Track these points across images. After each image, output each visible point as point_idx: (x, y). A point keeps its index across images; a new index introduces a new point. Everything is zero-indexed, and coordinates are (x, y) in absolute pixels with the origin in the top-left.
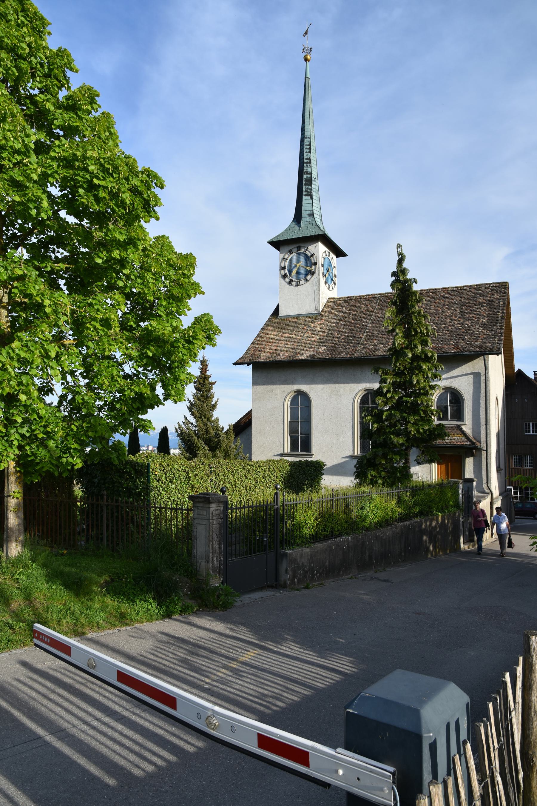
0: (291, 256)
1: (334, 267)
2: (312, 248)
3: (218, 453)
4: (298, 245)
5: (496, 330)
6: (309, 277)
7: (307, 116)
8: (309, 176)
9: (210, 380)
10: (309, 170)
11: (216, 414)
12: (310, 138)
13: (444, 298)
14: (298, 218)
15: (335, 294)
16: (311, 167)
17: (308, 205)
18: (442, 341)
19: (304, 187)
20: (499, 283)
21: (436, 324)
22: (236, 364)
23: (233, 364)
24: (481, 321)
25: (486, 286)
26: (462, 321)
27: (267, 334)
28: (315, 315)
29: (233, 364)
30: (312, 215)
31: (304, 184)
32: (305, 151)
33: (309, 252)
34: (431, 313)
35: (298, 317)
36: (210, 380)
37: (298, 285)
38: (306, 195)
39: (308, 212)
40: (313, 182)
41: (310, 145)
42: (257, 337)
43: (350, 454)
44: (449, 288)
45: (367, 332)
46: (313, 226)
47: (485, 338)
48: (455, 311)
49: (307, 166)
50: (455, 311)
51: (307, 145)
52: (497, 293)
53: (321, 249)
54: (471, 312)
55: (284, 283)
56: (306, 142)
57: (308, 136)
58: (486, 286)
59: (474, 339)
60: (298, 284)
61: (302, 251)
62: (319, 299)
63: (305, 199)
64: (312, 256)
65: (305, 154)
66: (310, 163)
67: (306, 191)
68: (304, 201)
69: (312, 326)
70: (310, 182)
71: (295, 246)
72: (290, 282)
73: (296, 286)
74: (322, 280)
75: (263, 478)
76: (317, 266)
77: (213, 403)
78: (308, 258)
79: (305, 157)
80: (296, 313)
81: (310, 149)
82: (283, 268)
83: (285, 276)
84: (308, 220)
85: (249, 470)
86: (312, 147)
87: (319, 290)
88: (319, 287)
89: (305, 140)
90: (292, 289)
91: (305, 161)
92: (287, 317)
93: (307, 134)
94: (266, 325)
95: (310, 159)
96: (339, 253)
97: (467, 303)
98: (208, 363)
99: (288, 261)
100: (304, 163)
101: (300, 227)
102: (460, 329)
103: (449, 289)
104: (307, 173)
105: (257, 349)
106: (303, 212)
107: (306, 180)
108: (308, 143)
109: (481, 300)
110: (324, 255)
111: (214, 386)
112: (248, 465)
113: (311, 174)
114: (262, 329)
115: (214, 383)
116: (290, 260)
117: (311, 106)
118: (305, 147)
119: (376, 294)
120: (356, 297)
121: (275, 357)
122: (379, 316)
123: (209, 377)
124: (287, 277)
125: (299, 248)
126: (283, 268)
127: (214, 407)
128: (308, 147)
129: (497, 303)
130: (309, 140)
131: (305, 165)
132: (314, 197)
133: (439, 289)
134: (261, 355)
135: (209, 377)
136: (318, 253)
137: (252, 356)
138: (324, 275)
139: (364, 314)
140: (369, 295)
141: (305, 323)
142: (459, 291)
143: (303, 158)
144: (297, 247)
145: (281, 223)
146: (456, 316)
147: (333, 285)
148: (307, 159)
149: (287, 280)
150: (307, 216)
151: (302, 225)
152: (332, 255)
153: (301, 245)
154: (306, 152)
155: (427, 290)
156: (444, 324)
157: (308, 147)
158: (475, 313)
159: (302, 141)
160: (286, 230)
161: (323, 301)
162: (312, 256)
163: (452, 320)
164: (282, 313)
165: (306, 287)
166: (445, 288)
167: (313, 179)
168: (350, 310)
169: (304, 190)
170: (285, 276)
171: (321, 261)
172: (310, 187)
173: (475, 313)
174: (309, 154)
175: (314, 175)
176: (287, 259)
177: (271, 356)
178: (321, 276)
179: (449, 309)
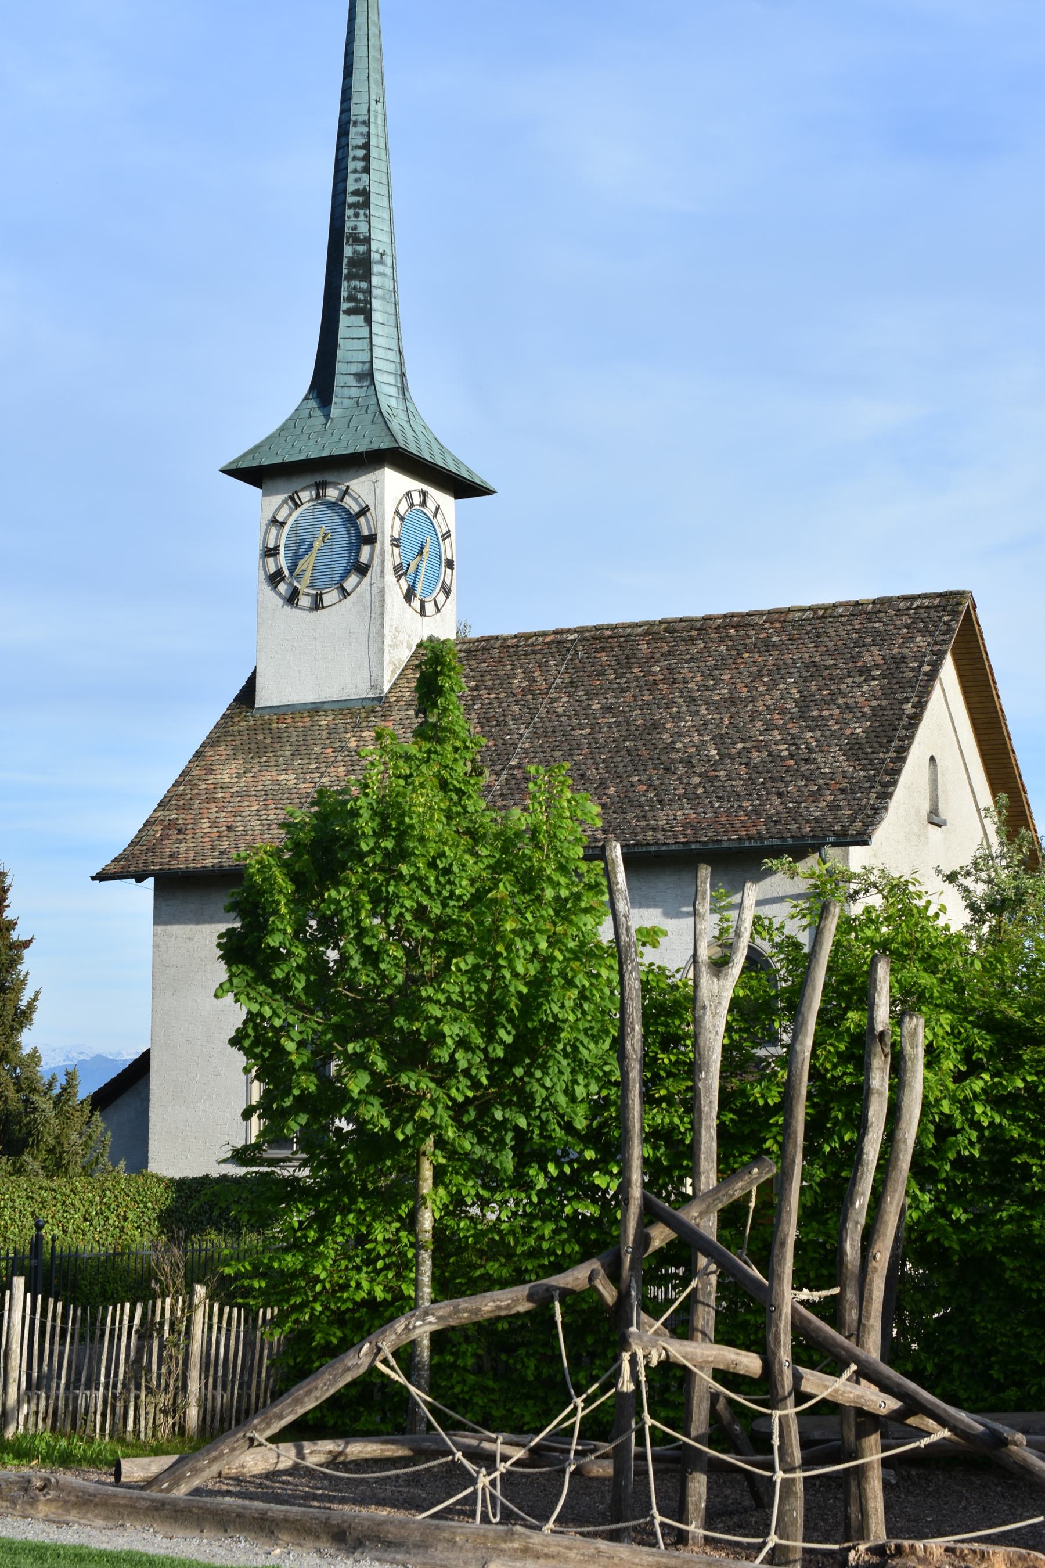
0: (296, 514)
1: (447, 535)
2: (360, 486)
3: (30, 1159)
4: (318, 478)
5: (883, 761)
6: (352, 581)
7: (360, 51)
8: (362, 249)
9: (15, 935)
10: (363, 228)
11: (28, 1039)
12: (367, 123)
13: (768, 646)
14: (322, 386)
15: (443, 627)
16: (368, 217)
17: (357, 345)
18: (719, 798)
19: (344, 284)
20: (940, 595)
21: (719, 740)
22: (101, 877)
23: (93, 878)
24: (848, 732)
25: (902, 605)
26: (793, 731)
27: (211, 771)
28: (368, 705)
29: (93, 878)
30: (367, 376)
31: (348, 272)
32: (352, 165)
33: (355, 499)
34: (715, 703)
35: (315, 709)
36: (15, 935)
37: (317, 608)
38: (349, 312)
39: (355, 368)
40: (375, 268)
41: (366, 146)
42: (177, 784)
44: (789, 610)
45: (513, 768)
46: (370, 416)
47: (843, 791)
48: (785, 695)
49: (357, 215)
50: (785, 695)
51: (359, 147)
52: (924, 632)
53: (394, 484)
54: (831, 701)
55: (272, 599)
56: (355, 138)
57: (361, 119)
58: (902, 605)
59: (812, 794)
60: (318, 604)
61: (332, 493)
62: (381, 651)
63: (348, 325)
64: (364, 511)
65: (351, 177)
66: (366, 204)
67: (351, 298)
68: (343, 332)
69: (353, 744)
70: (363, 267)
71: (311, 480)
73: (311, 609)
74: (395, 589)
75: (85, 1220)
76: (378, 545)
77: (23, 1003)
78: (352, 519)
79: (351, 186)
80: (309, 697)
81: (367, 158)
82: (270, 552)
84: (354, 392)
85: (43, 1202)
86: (374, 153)
87: (382, 625)
88: (382, 614)
89: (353, 130)
90: (300, 618)
91: (351, 199)
92: (281, 712)
93: (358, 111)
94: (211, 742)
95: (365, 193)
96: (462, 487)
97: (827, 668)
98: (8, 881)
99: (287, 528)
100: (347, 203)
101: (327, 416)
102: (783, 759)
103: (791, 616)
104: (356, 239)
105: (172, 824)
106: (340, 367)
107: (352, 263)
108: (361, 141)
109: (872, 656)
110: (403, 508)
111: (26, 952)
112: (40, 1188)
113: (367, 240)
114: (198, 755)
115: (27, 944)
116: (295, 527)
117: (373, 17)
118: (351, 154)
119: (568, 631)
120: (505, 639)
121: (222, 853)
122: (560, 710)
123: (12, 925)
124: (283, 579)
125: (322, 486)
126: (270, 552)
127: (23, 1017)
128: (361, 153)
129: (913, 670)
130: (365, 130)
131: (349, 212)
132: (376, 316)
133: (761, 614)
134: (183, 847)
135: (12, 925)
136: (382, 504)
137: (152, 850)
138: (400, 571)
139: (517, 702)
140: (544, 634)
141: (332, 731)
142: (821, 618)
143: (345, 191)
145: (269, 399)
146: (783, 712)
147: (441, 598)
148: (356, 193)
150: (351, 381)
151: (335, 412)
152: (438, 497)
153: (329, 477)
154: (355, 171)
155: (725, 616)
156: (743, 741)
157: (361, 153)
158: (841, 701)
159: (343, 132)
160: (282, 429)
161: (398, 654)
162: (364, 511)
163: (770, 727)
164: (264, 698)
165: (340, 614)
166: (779, 612)
167: (375, 257)
168: (477, 688)
169: (344, 294)
170: (275, 579)
171: (389, 527)
172: (364, 285)
173: (841, 701)
174: (365, 176)
175: (379, 241)
176: (283, 524)
177: (213, 848)
178: (390, 577)
179: (771, 687)
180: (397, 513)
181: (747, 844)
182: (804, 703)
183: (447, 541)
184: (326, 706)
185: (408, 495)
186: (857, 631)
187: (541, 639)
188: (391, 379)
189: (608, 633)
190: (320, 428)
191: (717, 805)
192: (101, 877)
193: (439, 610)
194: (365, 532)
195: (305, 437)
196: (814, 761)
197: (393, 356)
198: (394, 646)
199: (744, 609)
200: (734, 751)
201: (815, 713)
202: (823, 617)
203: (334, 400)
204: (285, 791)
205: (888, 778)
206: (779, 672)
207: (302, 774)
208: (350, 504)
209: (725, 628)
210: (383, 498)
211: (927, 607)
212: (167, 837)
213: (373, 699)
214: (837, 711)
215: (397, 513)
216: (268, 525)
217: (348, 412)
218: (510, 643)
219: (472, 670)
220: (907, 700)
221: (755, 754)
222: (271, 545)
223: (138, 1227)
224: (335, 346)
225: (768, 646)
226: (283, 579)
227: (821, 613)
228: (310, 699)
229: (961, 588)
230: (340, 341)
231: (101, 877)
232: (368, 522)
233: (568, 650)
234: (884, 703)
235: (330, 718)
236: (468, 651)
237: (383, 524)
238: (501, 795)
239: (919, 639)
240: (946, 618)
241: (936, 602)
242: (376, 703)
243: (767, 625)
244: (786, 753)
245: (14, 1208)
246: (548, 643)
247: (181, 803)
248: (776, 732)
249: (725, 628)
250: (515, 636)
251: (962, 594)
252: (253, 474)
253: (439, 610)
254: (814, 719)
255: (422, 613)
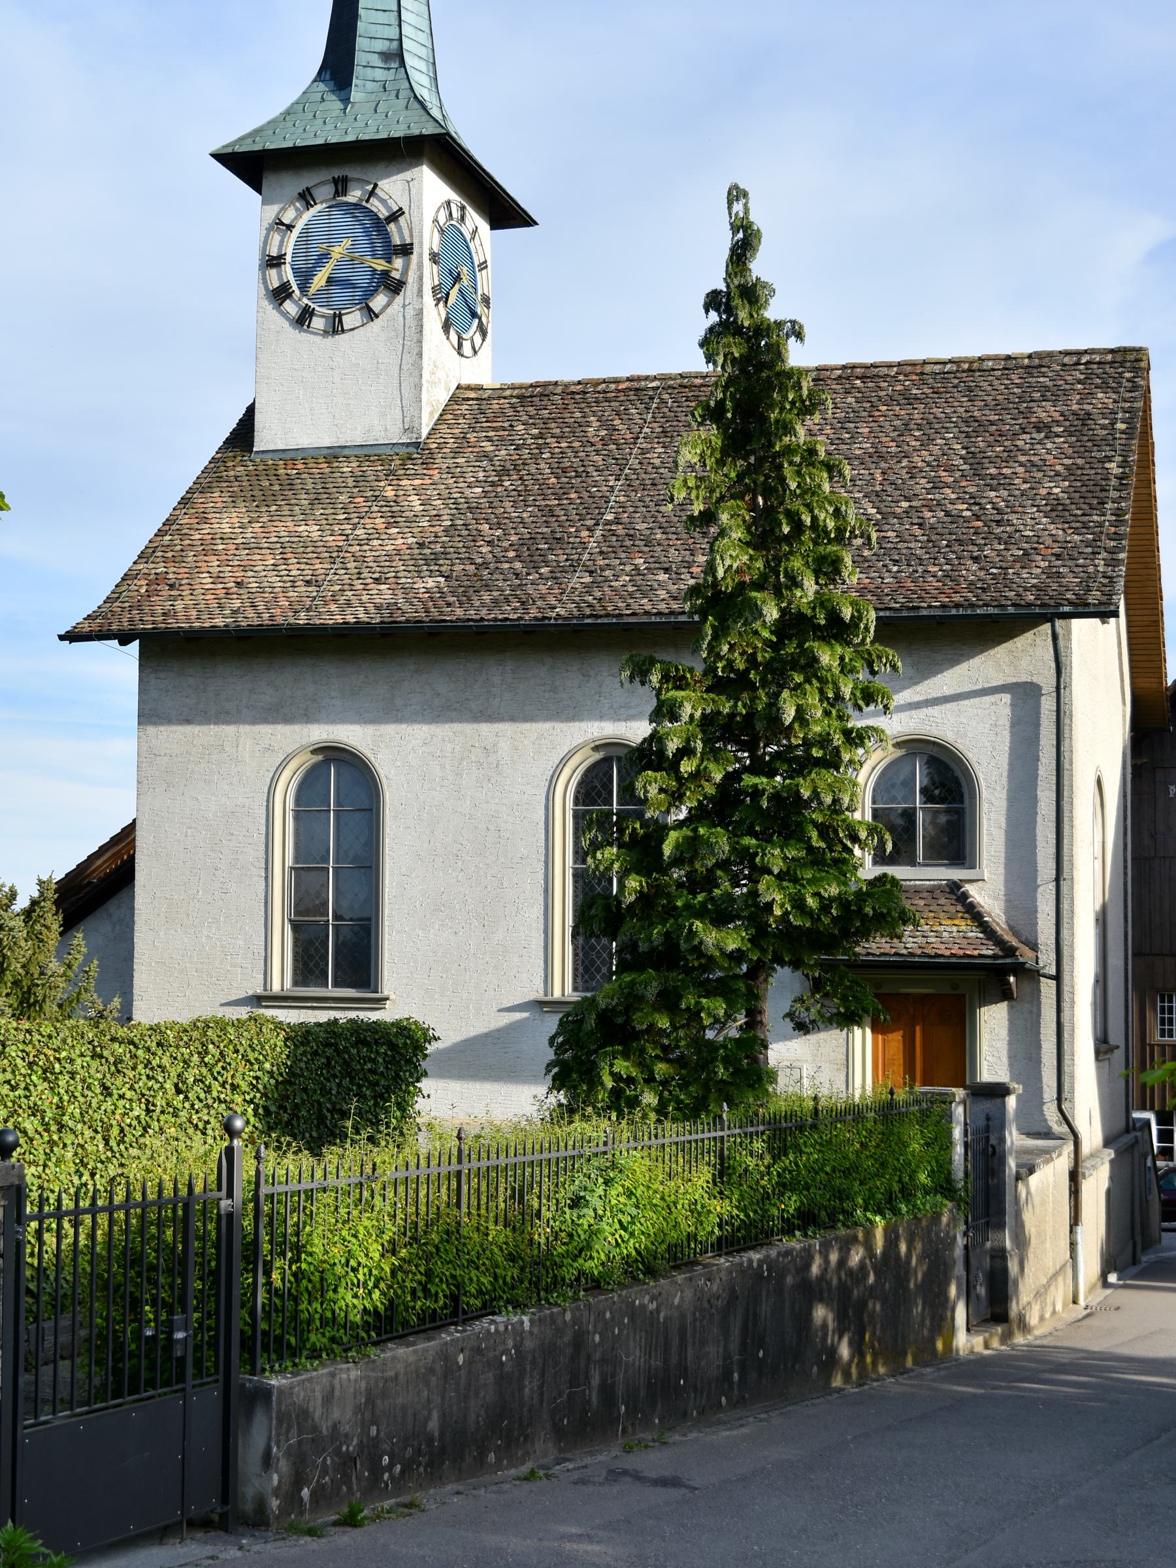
0: (307, 216)
4: (337, 173)
6: (379, 301)
13: (910, 400)
14: (338, 66)
15: (482, 371)
17: (381, 17)
20: (1112, 351)
21: (876, 497)
23: (62, 638)
24: (1043, 492)
25: (1066, 360)
28: (403, 451)
29: (62, 638)
30: (395, 56)
33: (383, 202)
35: (333, 455)
37: (335, 332)
39: (381, 46)
42: (160, 533)
43: (533, 996)
45: (608, 523)
46: (402, 102)
47: (1058, 556)
55: (276, 321)
62: (418, 387)
64: (394, 217)
69: (390, 493)
72: (303, 319)
74: (434, 316)
75: (178, 1091)
76: (414, 258)
83: (280, 294)
84: (380, 74)
88: (420, 342)
90: (312, 345)
92: (289, 457)
94: (201, 486)
96: (504, 212)
97: (992, 423)
99: (296, 232)
105: (159, 579)
106: (360, 43)
109: (1046, 412)
110: (442, 218)
112: (113, 1039)
114: (185, 502)
116: (306, 232)
119: (647, 378)
120: (567, 385)
121: (234, 612)
122: (657, 462)
124: (289, 295)
125: (341, 186)
126: (274, 262)
129: (1103, 427)
136: (420, 207)
140: (616, 381)
144: (335, 181)
146: (950, 469)
147: (478, 339)
149: (291, 308)
150: (376, 60)
151: (356, 95)
153: (351, 172)
155: (844, 367)
158: (1023, 459)
160: (288, 113)
162: (394, 217)
165: (366, 342)
168: (541, 436)
171: (428, 240)
173: (1023, 459)
176: (290, 227)
180: (436, 221)
181: (954, 612)
182: (975, 460)
183: (484, 272)
184: (346, 452)
185: (448, 203)
186: (1018, 386)
187: (613, 386)
188: (422, 66)
189: (698, 381)
190: (337, 113)
191: (895, 569)
192: (72, 637)
193: (475, 352)
194: (397, 240)
195: (319, 121)
196: (1009, 523)
197: (423, 38)
198: (432, 383)
199: (869, 360)
200: (899, 510)
201: (993, 471)
202: (970, 370)
203: (354, 81)
204: (306, 543)
205: (1112, 543)
206: (930, 429)
207: (327, 525)
208: (375, 205)
209: (848, 378)
210: (420, 200)
211: (1099, 363)
212: (157, 593)
213: (408, 445)
214: (1021, 470)
215: (436, 221)
216: (269, 229)
217: (373, 97)
218: (573, 388)
219: (531, 417)
220: (1109, 459)
221: (928, 514)
222: (274, 253)
223: (251, 1101)
224: (354, 17)
225: (910, 400)
226: (289, 295)
227: (966, 366)
228: (327, 443)
229: (1137, 345)
230: (361, 12)
231: (72, 637)
232: (400, 229)
233: (652, 398)
234: (1080, 461)
235: (355, 464)
236: (521, 397)
237: (421, 232)
238: (601, 553)
239: (1100, 395)
240: (1127, 375)
241: (1109, 357)
242: (412, 449)
243: (901, 377)
244: (968, 513)
245: (73, 1075)
246: (623, 390)
247: (170, 554)
248: (948, 491)
249: (848, 378)
250: (579, 383)
251: (1139, 350)
252: (250, 165)
253: (475, 352)
254: (993, 477)
255: (459, 349)
